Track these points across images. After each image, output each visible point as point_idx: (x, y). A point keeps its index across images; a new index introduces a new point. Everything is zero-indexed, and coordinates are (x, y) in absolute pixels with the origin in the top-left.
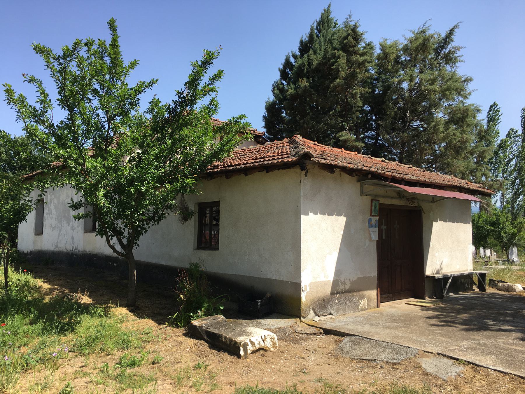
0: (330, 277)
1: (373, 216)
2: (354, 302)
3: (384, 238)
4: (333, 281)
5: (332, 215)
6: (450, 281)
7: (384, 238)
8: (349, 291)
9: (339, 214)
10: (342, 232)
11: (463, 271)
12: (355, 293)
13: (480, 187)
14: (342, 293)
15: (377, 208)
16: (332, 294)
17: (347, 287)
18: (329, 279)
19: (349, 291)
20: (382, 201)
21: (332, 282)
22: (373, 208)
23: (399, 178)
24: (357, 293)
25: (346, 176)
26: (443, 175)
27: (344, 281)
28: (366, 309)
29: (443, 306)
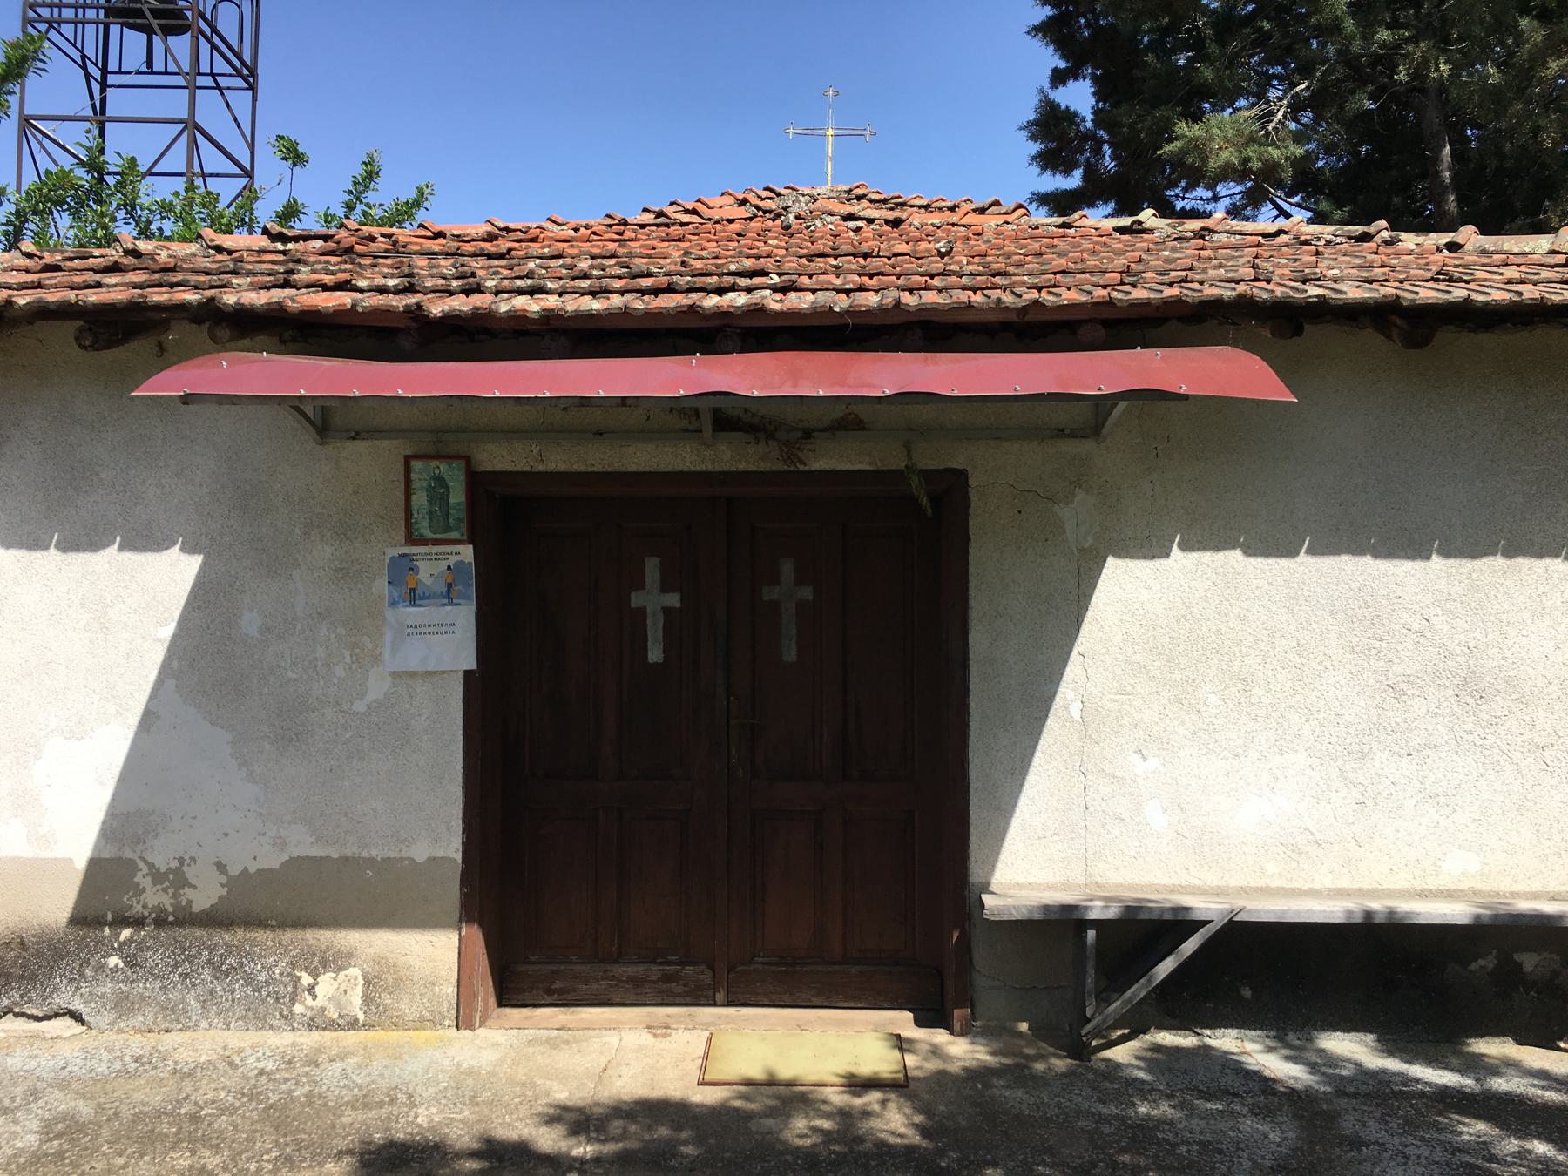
0: (75, 837)
1: (423, 542)
2: (250, 980)
3: (655, 654)
4: (93, 863)
5: (94, 546)
6: (1190, 946)
7: (655, 654)
8: (215, 919)
9: (145, 539)
10: (168, 631)
11: (1245, 891)
12: (263, 937)
13: (382, 290)
14: (160, 922)
15: (458, 496)
16: (77, 920)
17: (203, 897)
18: (59, 852)
19: (215, 919)
20: (498, 458)
21: (81, 864)
22: (420, 500)
23: (847, 312)
24: (287, 936)
25: (1370, 337)
26: (1489, 242)
27: (178, 872)
28: (353, 1025)
29: (1209, 1105)
